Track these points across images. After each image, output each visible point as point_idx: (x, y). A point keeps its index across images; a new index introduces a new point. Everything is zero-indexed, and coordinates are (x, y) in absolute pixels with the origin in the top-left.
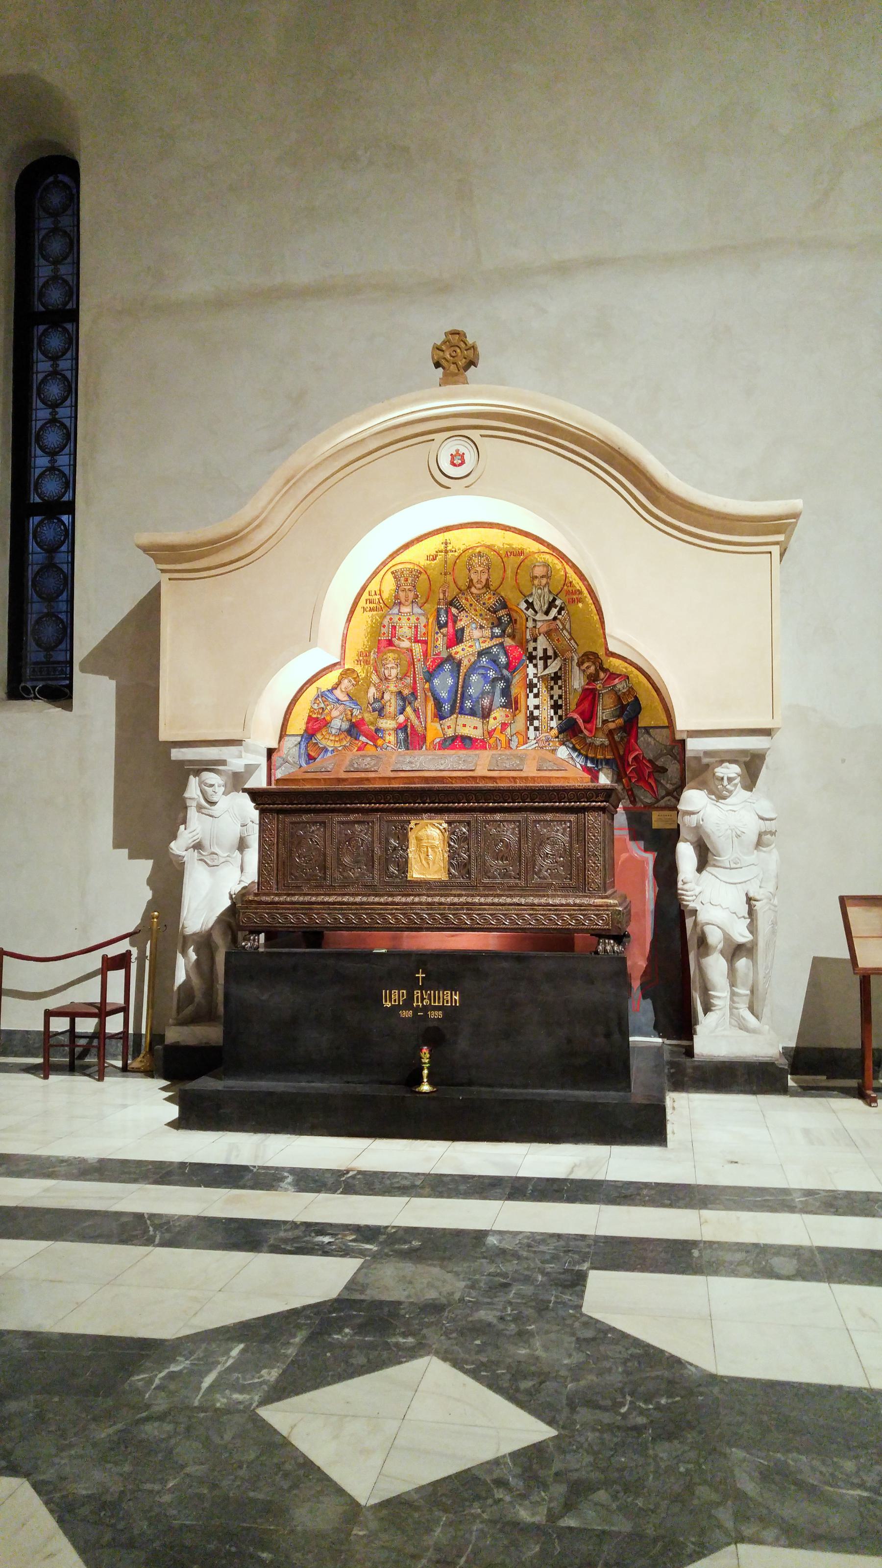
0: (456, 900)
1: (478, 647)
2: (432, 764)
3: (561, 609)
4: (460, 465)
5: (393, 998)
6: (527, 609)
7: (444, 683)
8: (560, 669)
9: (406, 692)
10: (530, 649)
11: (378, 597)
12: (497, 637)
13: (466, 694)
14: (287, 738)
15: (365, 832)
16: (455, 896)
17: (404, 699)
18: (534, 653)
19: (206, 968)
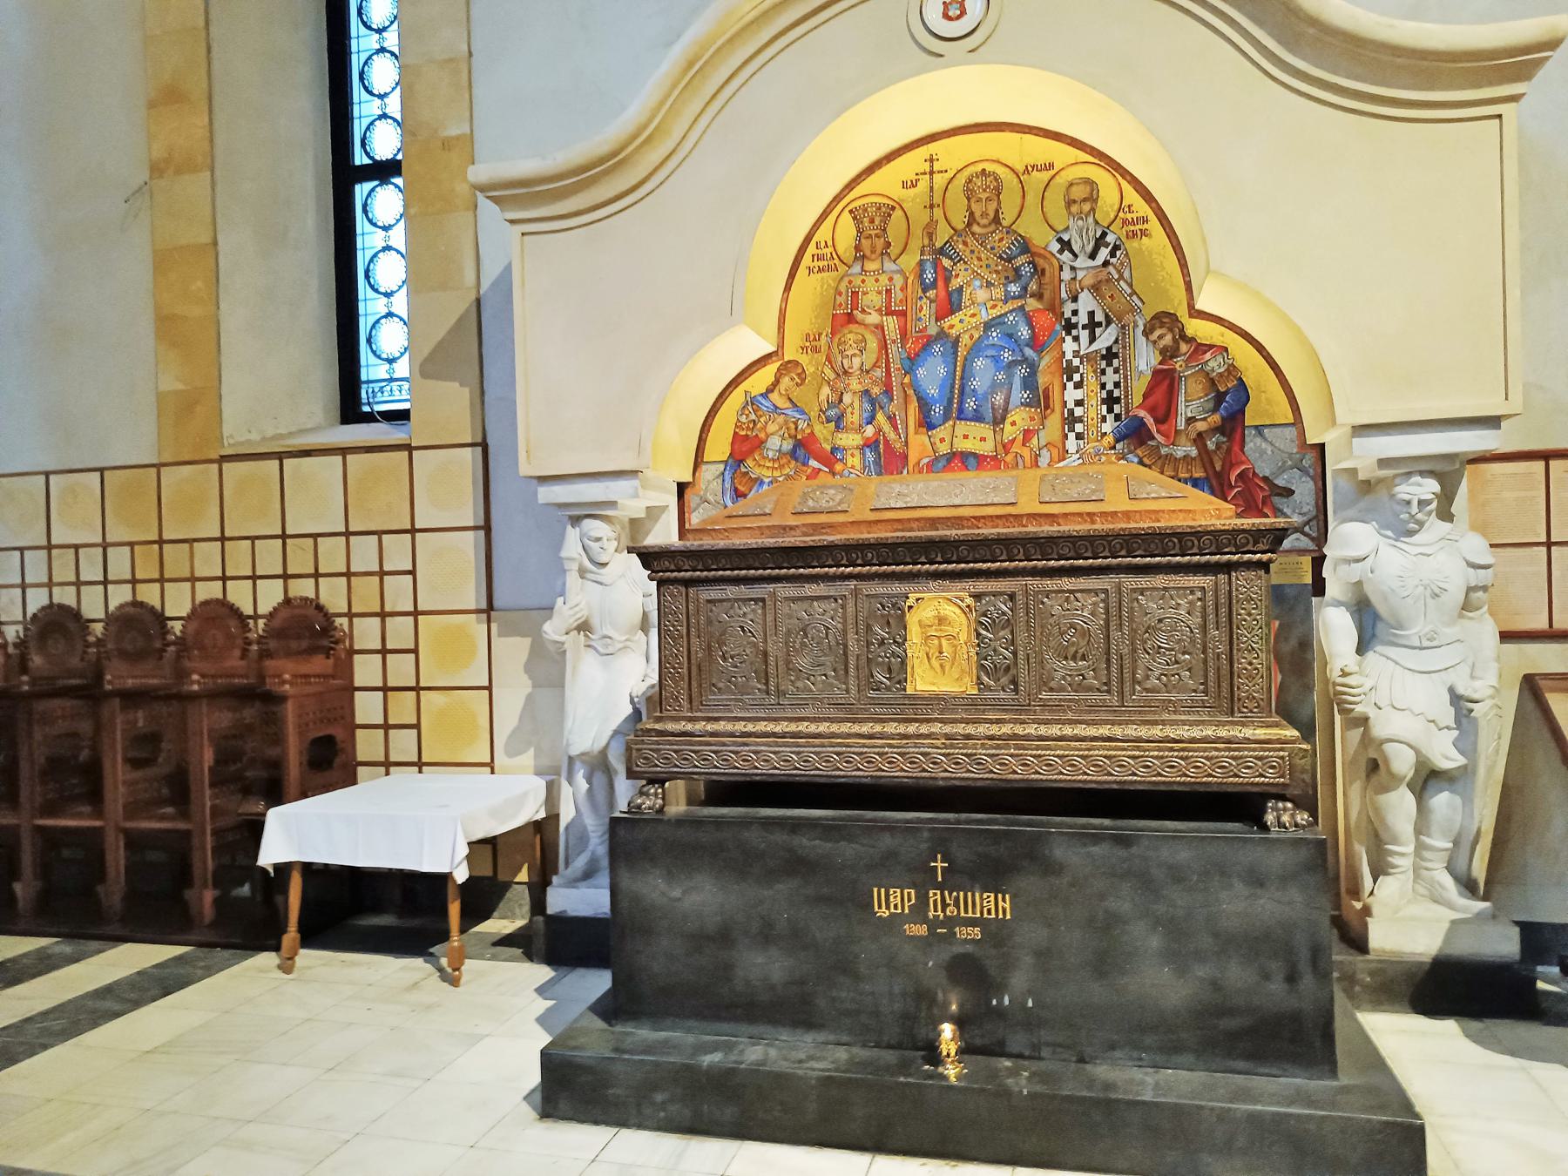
0: (994, 730)
1: (984, 316)
2: (928, 497)
3: (1116, 248)
4: (958, 17)
5: (891, 901)
6: (1061, 251)
7: (932, 374)
8: (1116, 341)
9: (876, 390)
10: (1068, 314)
11: (831, 249)
12: (1014, 298)
13: (967, 389)
14: (704, 467)
15: (820, 607)
16: (991, 722)
17: (873, 402)
18: (1074, 320)
19: (601, 796)
